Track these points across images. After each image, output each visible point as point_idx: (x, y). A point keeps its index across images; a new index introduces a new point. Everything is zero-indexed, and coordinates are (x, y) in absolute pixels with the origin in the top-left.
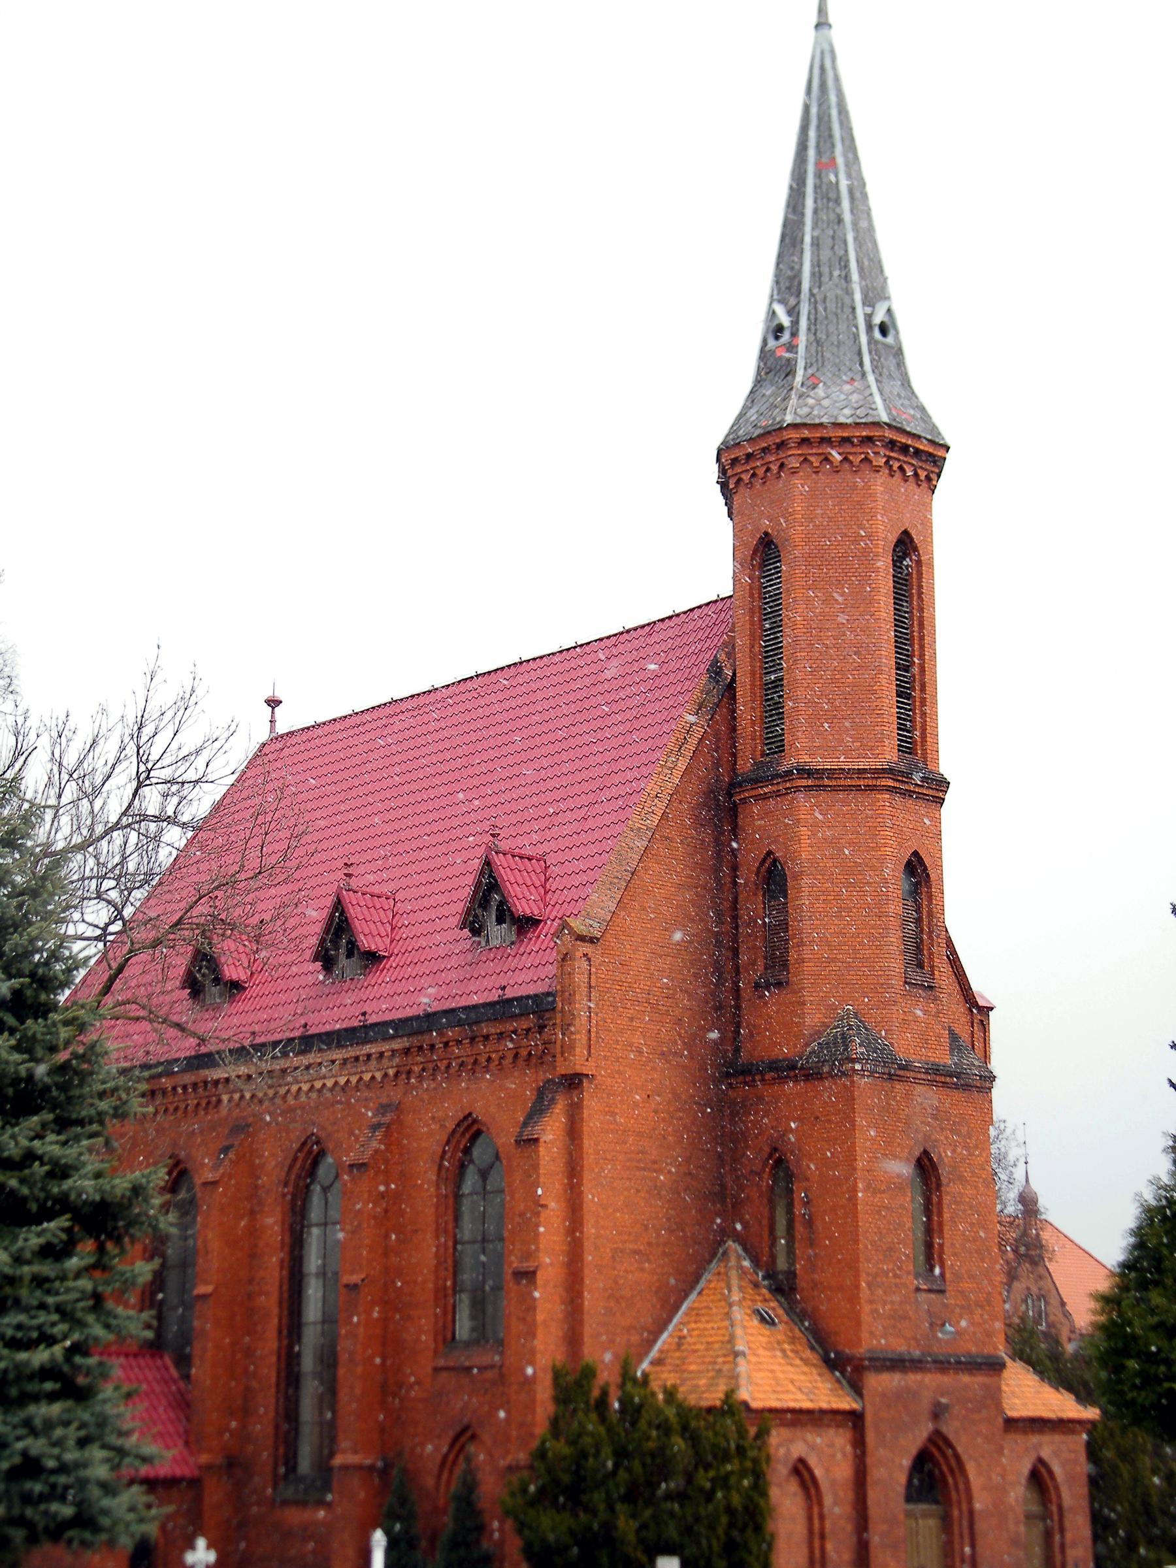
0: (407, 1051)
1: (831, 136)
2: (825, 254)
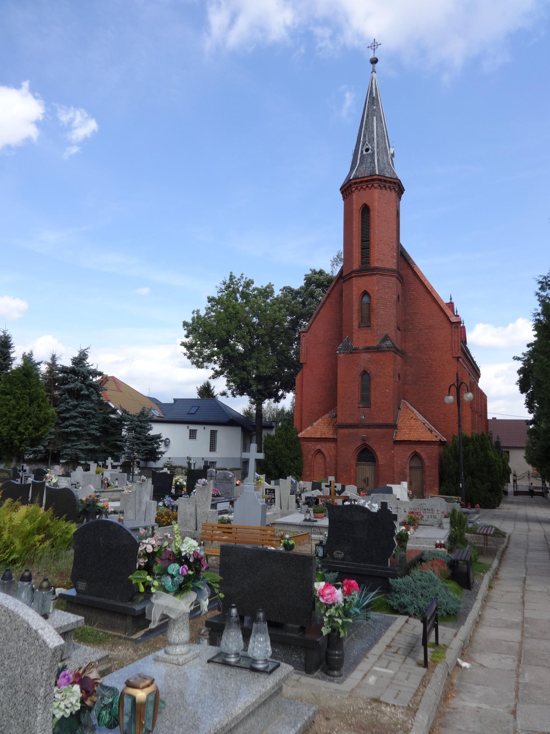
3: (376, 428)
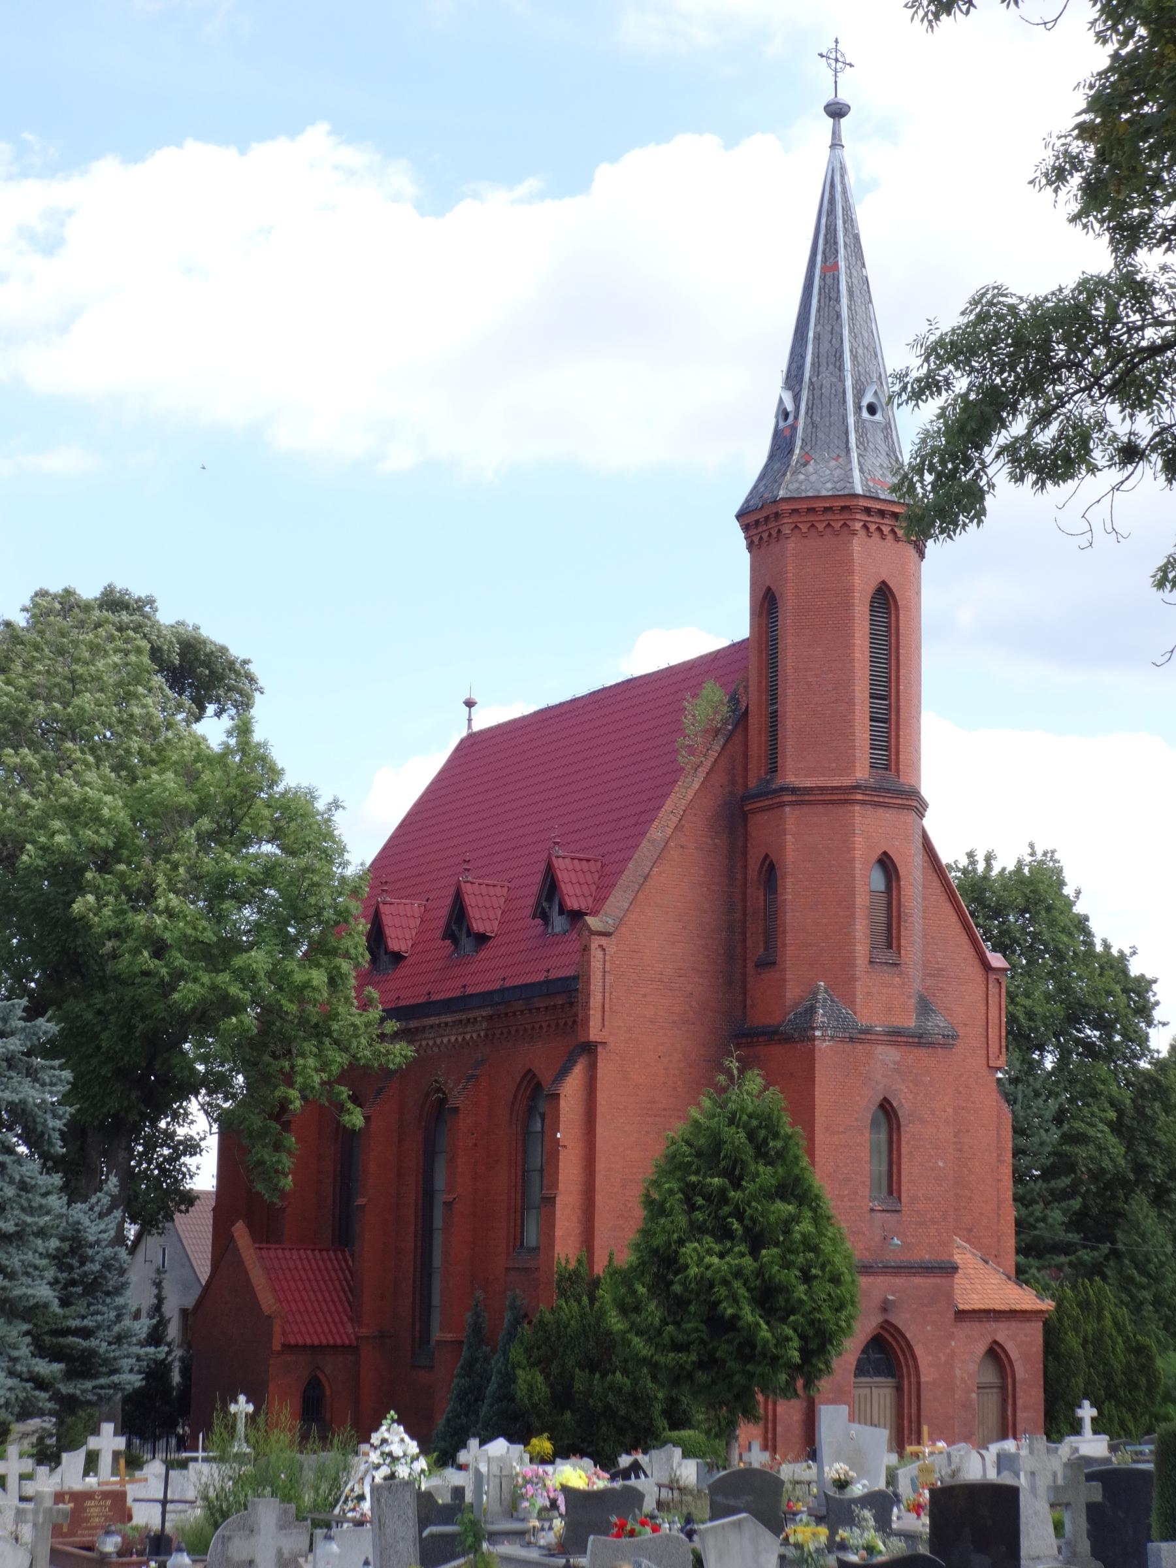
0: (490, 1018)
1: (836, 243)
2: (825, 346)
3: (914, 1274)
